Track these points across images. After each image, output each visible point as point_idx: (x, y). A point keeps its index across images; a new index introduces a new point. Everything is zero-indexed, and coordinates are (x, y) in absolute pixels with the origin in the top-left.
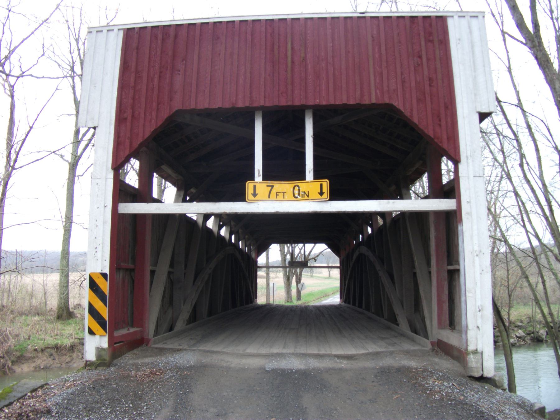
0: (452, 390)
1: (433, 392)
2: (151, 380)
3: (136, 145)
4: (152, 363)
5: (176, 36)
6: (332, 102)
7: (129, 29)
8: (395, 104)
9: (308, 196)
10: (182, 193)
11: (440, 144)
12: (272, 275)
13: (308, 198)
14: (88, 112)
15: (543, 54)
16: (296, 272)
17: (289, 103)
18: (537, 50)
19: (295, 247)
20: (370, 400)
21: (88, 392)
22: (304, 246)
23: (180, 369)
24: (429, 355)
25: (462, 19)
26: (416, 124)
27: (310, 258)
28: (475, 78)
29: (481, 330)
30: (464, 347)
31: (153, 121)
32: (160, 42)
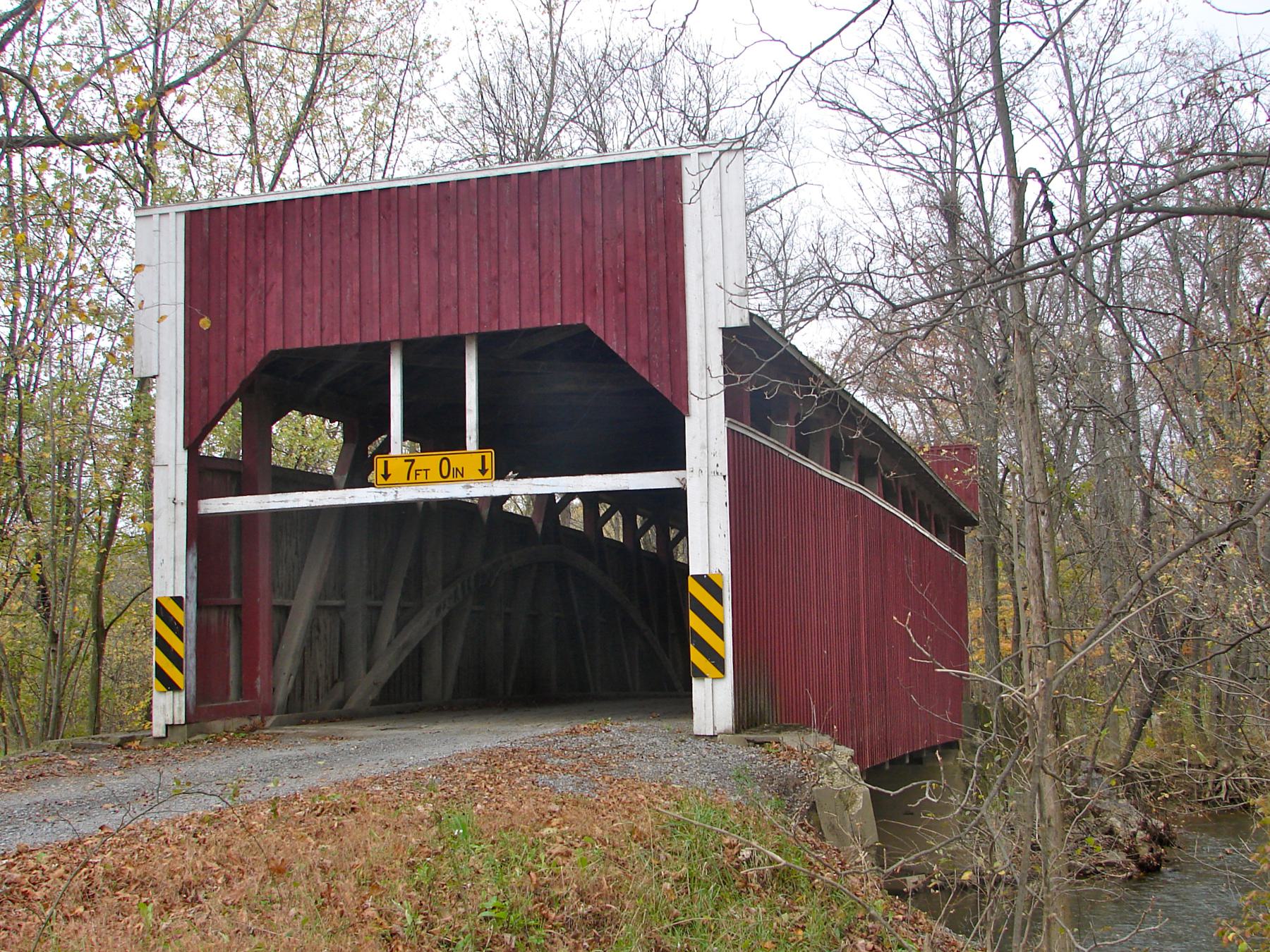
9: (462, 475)
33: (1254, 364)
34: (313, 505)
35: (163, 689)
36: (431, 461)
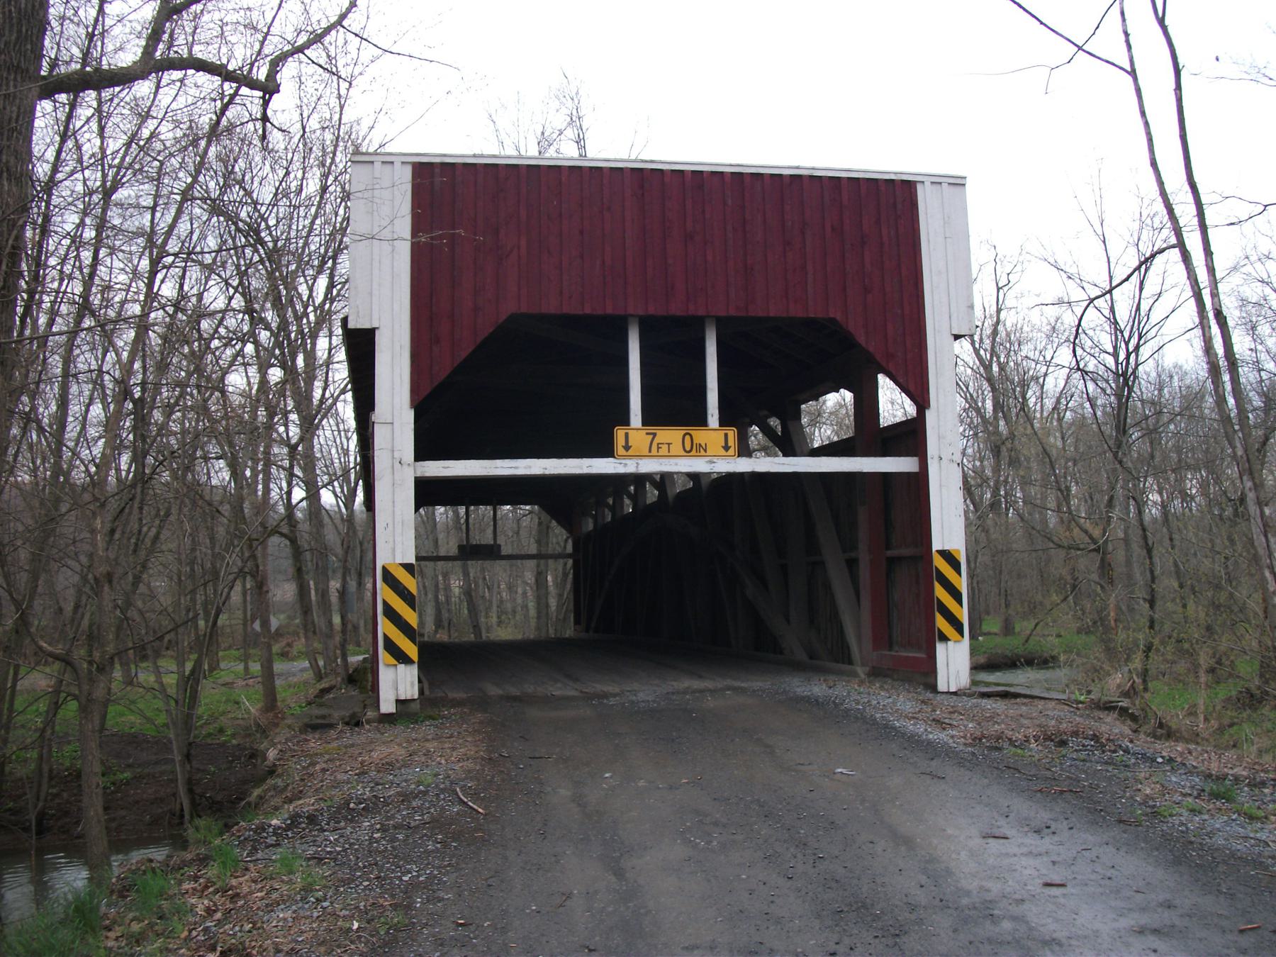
33: (309, 341)
34: (547, 472)
35: (393, 661)
36: (670, 435)
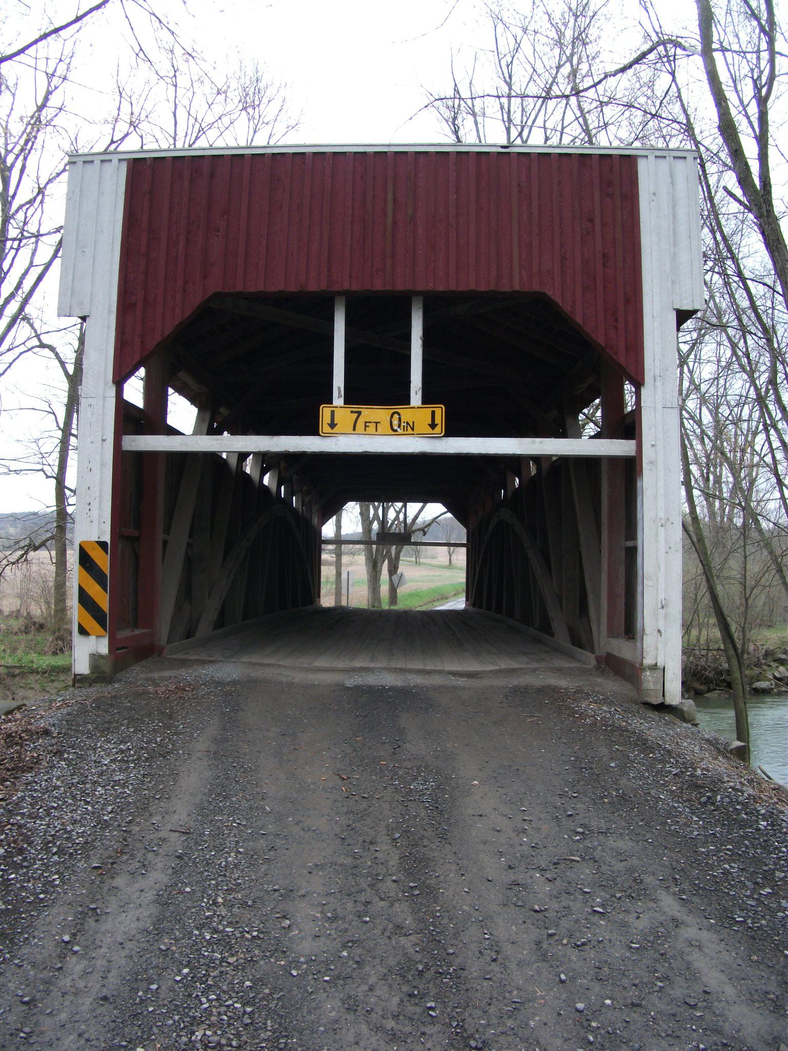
0: (613, 715)
1: (583, 716)
2: (180, 697)
3: (151, 344)
4: (175, 677)
5: (212, 175)
6: (453, 287)
7: (136, 160)
8: (550, 293)
9: (413, 429)
10: (207, 416)
11: (615, 357)
12: (345, 559)
13: (413, 432)
14: (72, 292)
15: (772, 229)
16: (389, 552)
17: (388, 288)
18: (764, 221)
19: (389, 508)
20: (494, 723)
21: (92, 712)
22: (405, 506)
23: (220, 683)
24: (591, 674)
25: (661, 161)
26: (580, 326)
27: (414, 528)
28: (674, 257)
29: (663, 636)
30: (639, 660)
31: (177, 310)
32: (186, 183)
36: (380, 414)
